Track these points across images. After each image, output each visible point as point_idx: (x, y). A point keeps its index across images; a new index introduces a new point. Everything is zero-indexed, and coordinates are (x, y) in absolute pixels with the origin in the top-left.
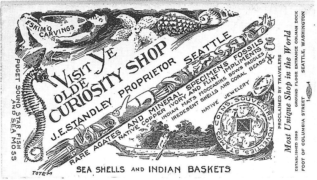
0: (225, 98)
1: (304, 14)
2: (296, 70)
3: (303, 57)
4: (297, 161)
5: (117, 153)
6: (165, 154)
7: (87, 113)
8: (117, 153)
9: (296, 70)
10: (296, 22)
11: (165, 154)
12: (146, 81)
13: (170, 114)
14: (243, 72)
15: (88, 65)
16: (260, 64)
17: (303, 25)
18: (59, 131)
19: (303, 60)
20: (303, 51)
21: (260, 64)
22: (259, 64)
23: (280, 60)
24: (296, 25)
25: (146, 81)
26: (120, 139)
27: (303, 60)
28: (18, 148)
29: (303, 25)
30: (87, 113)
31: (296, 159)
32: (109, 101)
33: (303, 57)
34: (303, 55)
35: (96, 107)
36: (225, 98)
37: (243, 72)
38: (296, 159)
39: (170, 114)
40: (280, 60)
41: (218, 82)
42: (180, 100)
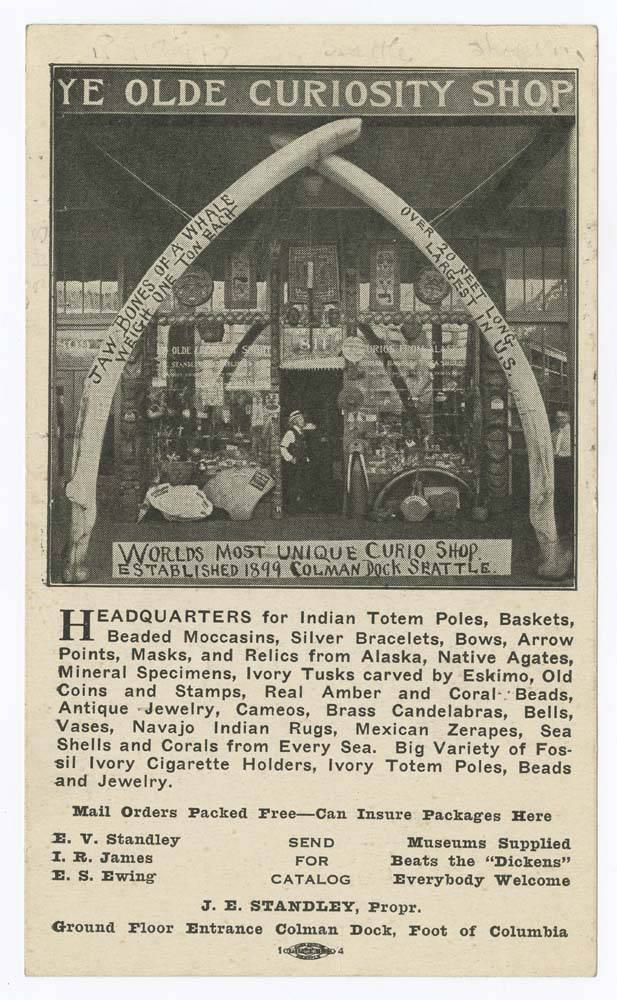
0: (99, 784)
2: (115, 811)
7: (67, 721)
9: (115, 811)
10: (518, 816)
12: (253, 759)
14: (319, 876)
16: (128, 620)
18: (282, 742)
20: (391, 931)
21: (128, 620)
22: (124, 616)
23: (232, 619)
24: (507, 816)
25: (253, 759)
28: (245, 759)
30: (67, 721)
36: (99, 784)
37: (319, 876)
40: (232, 619)
41: (302, 636)
42: (251, 761)
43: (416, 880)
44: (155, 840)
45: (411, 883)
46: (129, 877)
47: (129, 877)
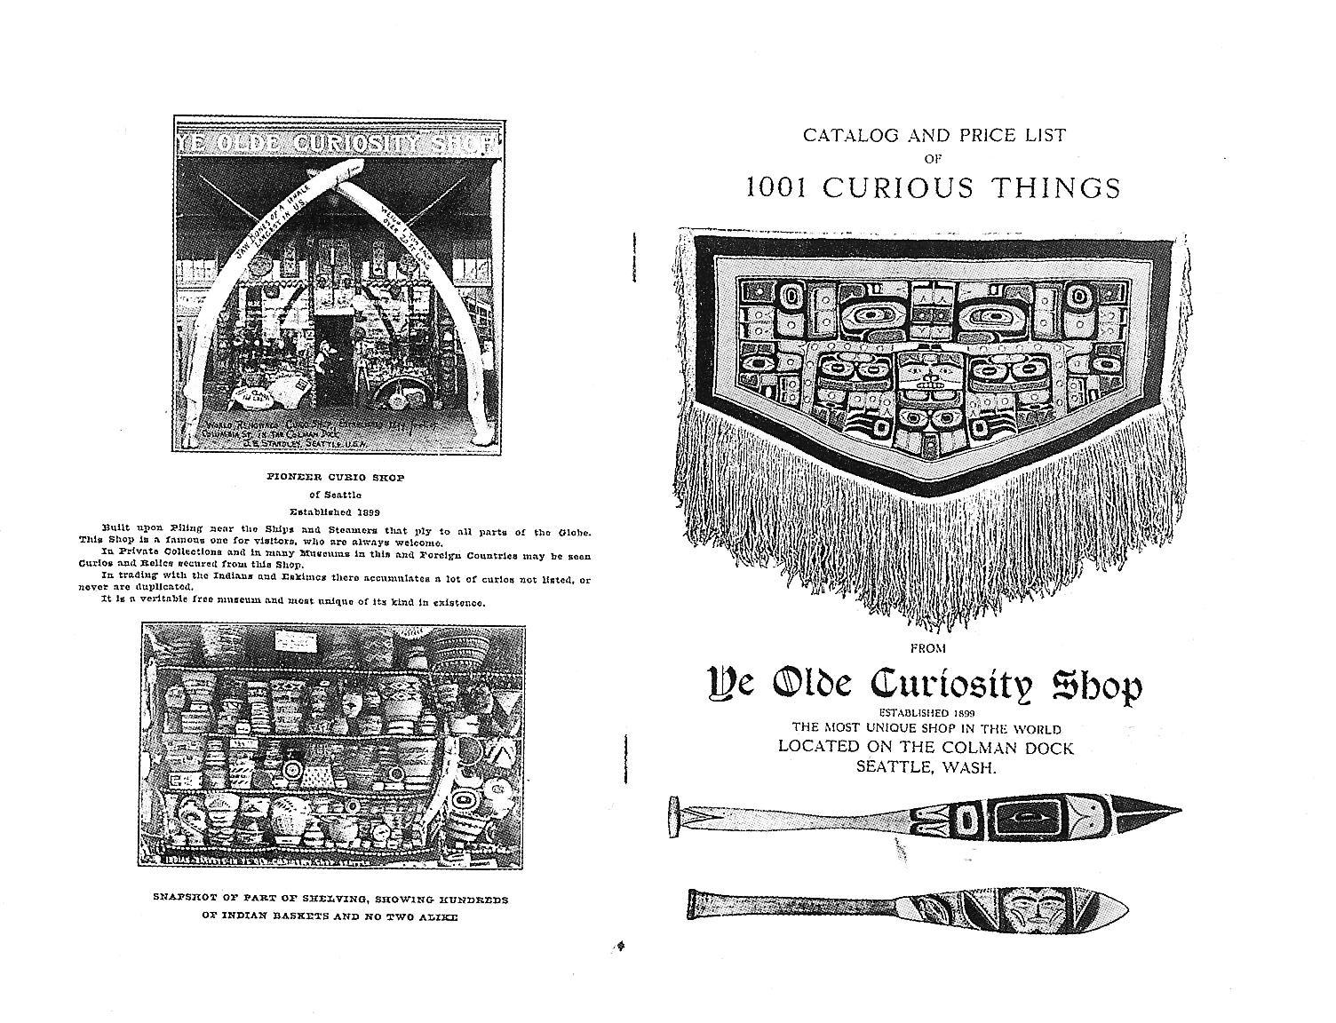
1: (885, 748)
3: (908, 766)
4: (260, 898)
5: (914, 131)
6: (987, 749)
8: (914, 131)
11: (987, 749)
13: (889, 726)
15: (895, 763)
17: (1077, 190)
19: (899, 767)
26: (1028, 703)
27: (899, 767)
29: (1077, 190)
31: (264, 898)
32: (1130, 699)
33: (908, 766)
34: (918, 766)
35: (970, 743)
38: (264, 898)
39: (889, 726)
43: (406, 917)
44: (231, 576)
45: (286, 914)
46: (172, 575)
47: (172, 575)
